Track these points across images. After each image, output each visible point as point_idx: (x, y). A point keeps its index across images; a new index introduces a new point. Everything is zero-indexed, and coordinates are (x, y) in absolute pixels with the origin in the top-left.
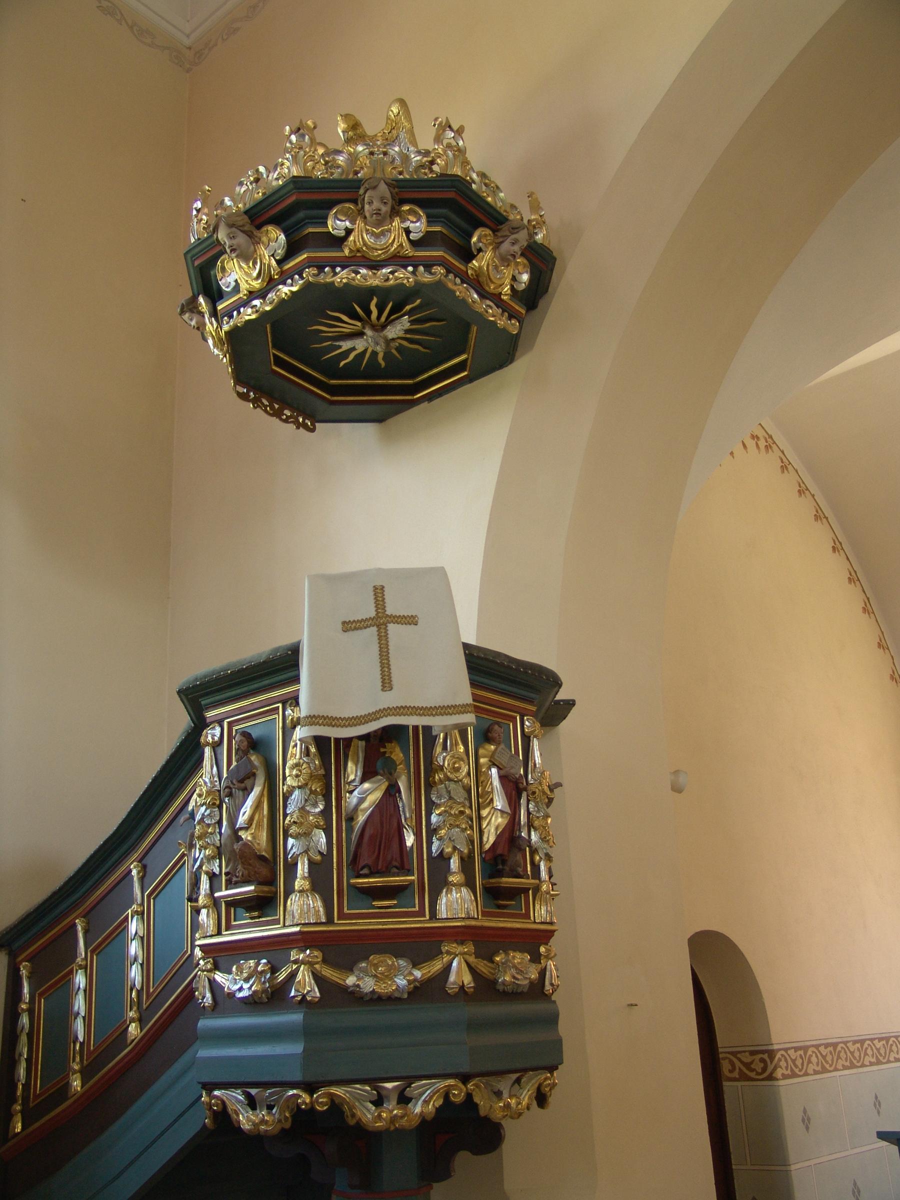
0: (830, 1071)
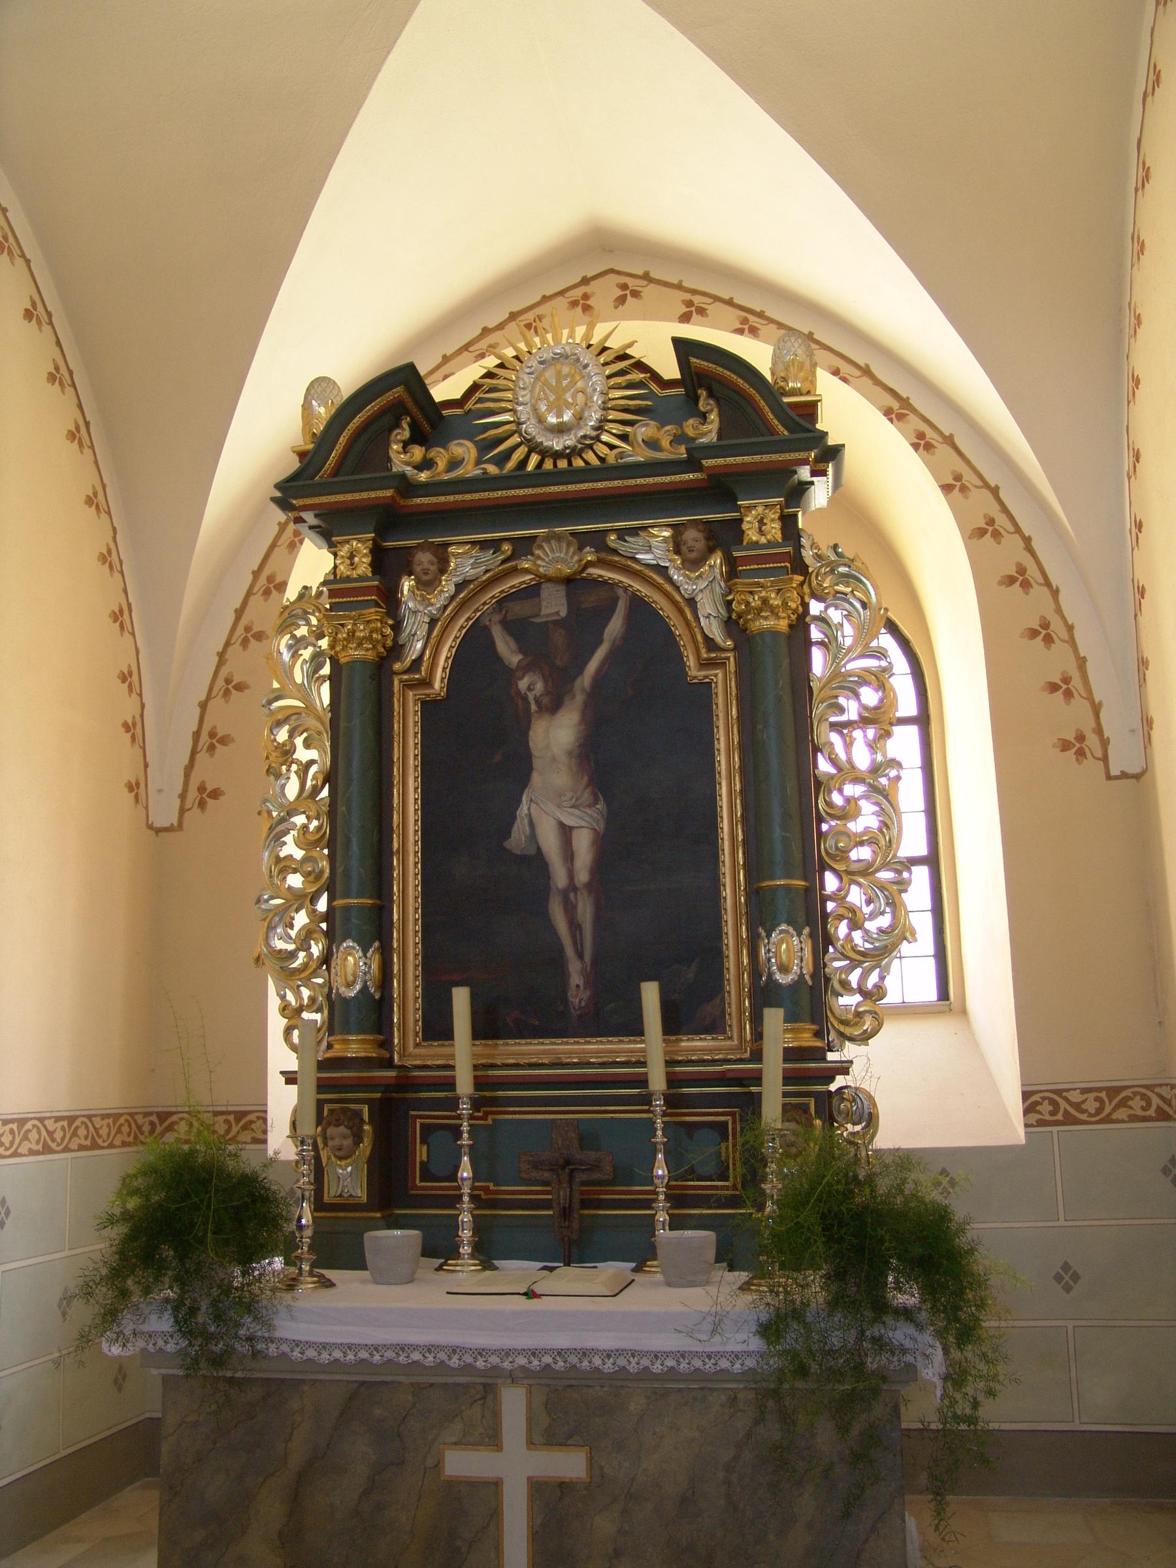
0: (103, 1148)
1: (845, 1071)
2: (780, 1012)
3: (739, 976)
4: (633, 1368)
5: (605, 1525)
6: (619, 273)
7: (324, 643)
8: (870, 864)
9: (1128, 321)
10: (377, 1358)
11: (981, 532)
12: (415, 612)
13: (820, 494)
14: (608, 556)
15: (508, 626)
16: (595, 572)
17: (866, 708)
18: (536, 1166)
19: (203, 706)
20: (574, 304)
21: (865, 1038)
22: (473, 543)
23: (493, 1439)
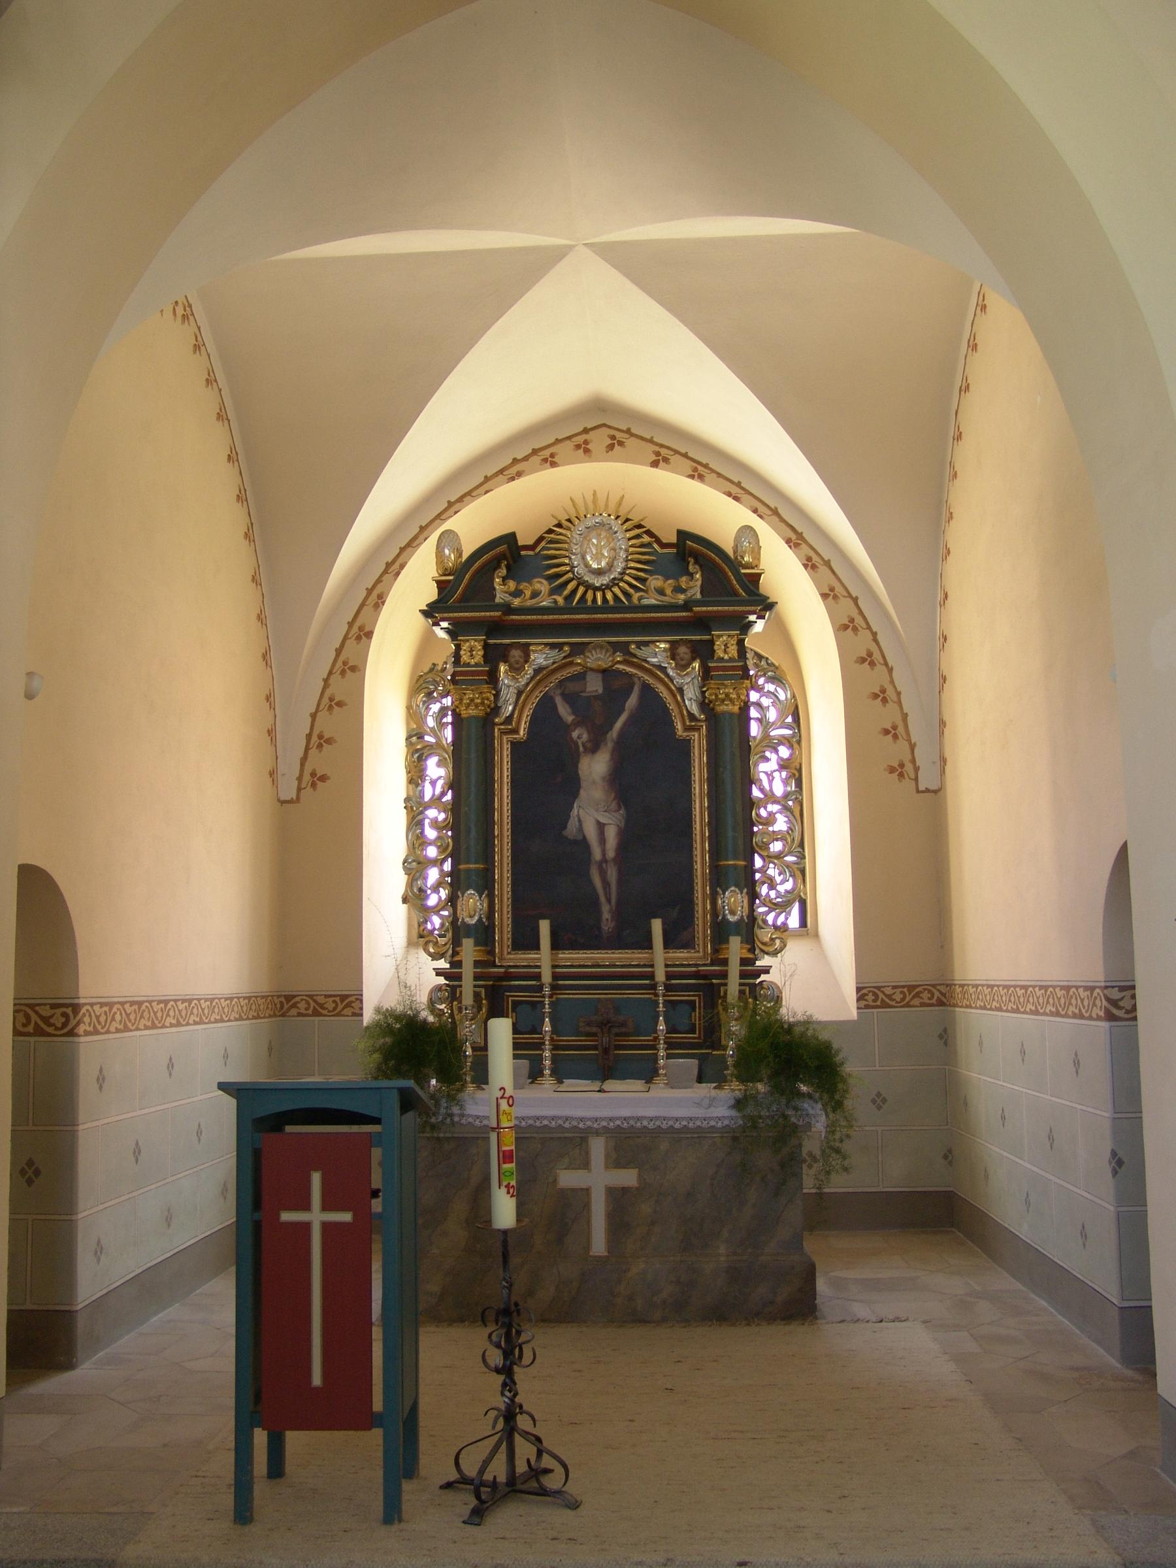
1: (767, 972)
2: (738, 939)
3: (705, 916)
4: (664, 1126)
5: (646, 1208)
6: (609, 427)
7: (448, 701)
8: (781, 852)
9: (944, 517)
10: (523, 1124)
11: (845, 627)
12: (509, 686)
13: (759, 626)
14: (629, 658)
15: (567, 698)
16: (621, 667)
17: (782, 759)
18: (589, 1024)
19: (314, 716)
20: (578, 447)
21: (775, 953)
22: (546, 644)
23: (586, 1165)
